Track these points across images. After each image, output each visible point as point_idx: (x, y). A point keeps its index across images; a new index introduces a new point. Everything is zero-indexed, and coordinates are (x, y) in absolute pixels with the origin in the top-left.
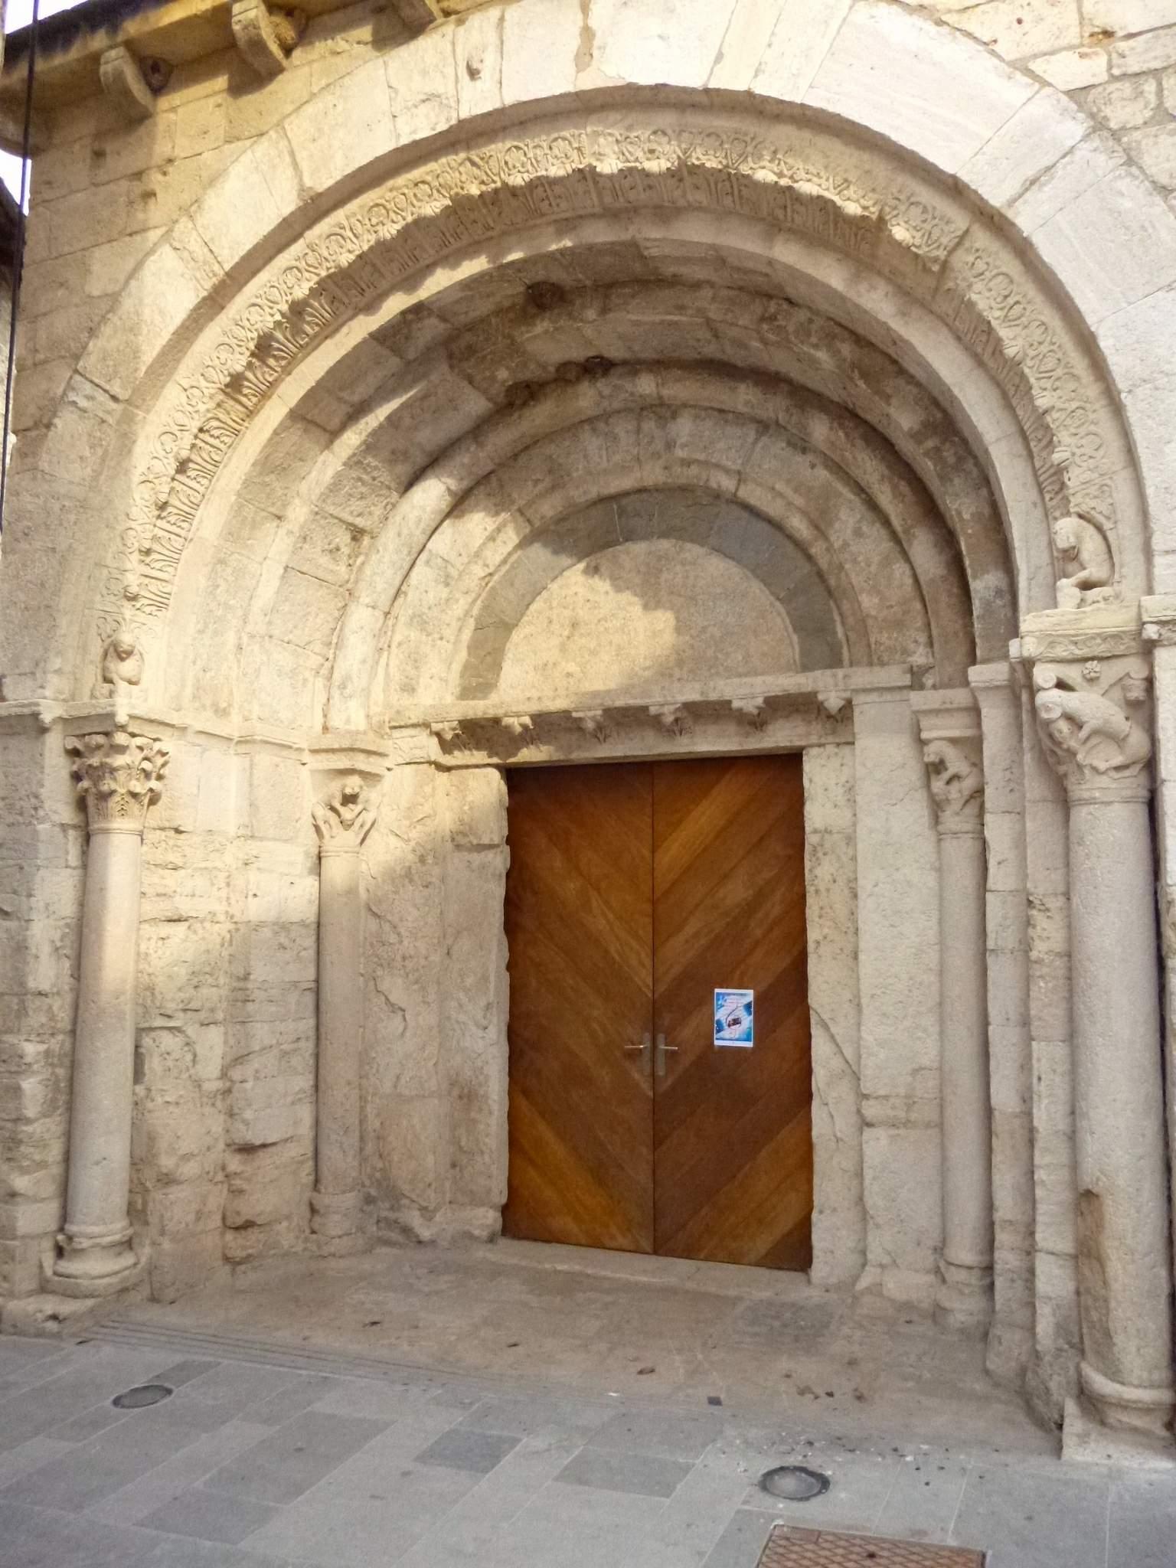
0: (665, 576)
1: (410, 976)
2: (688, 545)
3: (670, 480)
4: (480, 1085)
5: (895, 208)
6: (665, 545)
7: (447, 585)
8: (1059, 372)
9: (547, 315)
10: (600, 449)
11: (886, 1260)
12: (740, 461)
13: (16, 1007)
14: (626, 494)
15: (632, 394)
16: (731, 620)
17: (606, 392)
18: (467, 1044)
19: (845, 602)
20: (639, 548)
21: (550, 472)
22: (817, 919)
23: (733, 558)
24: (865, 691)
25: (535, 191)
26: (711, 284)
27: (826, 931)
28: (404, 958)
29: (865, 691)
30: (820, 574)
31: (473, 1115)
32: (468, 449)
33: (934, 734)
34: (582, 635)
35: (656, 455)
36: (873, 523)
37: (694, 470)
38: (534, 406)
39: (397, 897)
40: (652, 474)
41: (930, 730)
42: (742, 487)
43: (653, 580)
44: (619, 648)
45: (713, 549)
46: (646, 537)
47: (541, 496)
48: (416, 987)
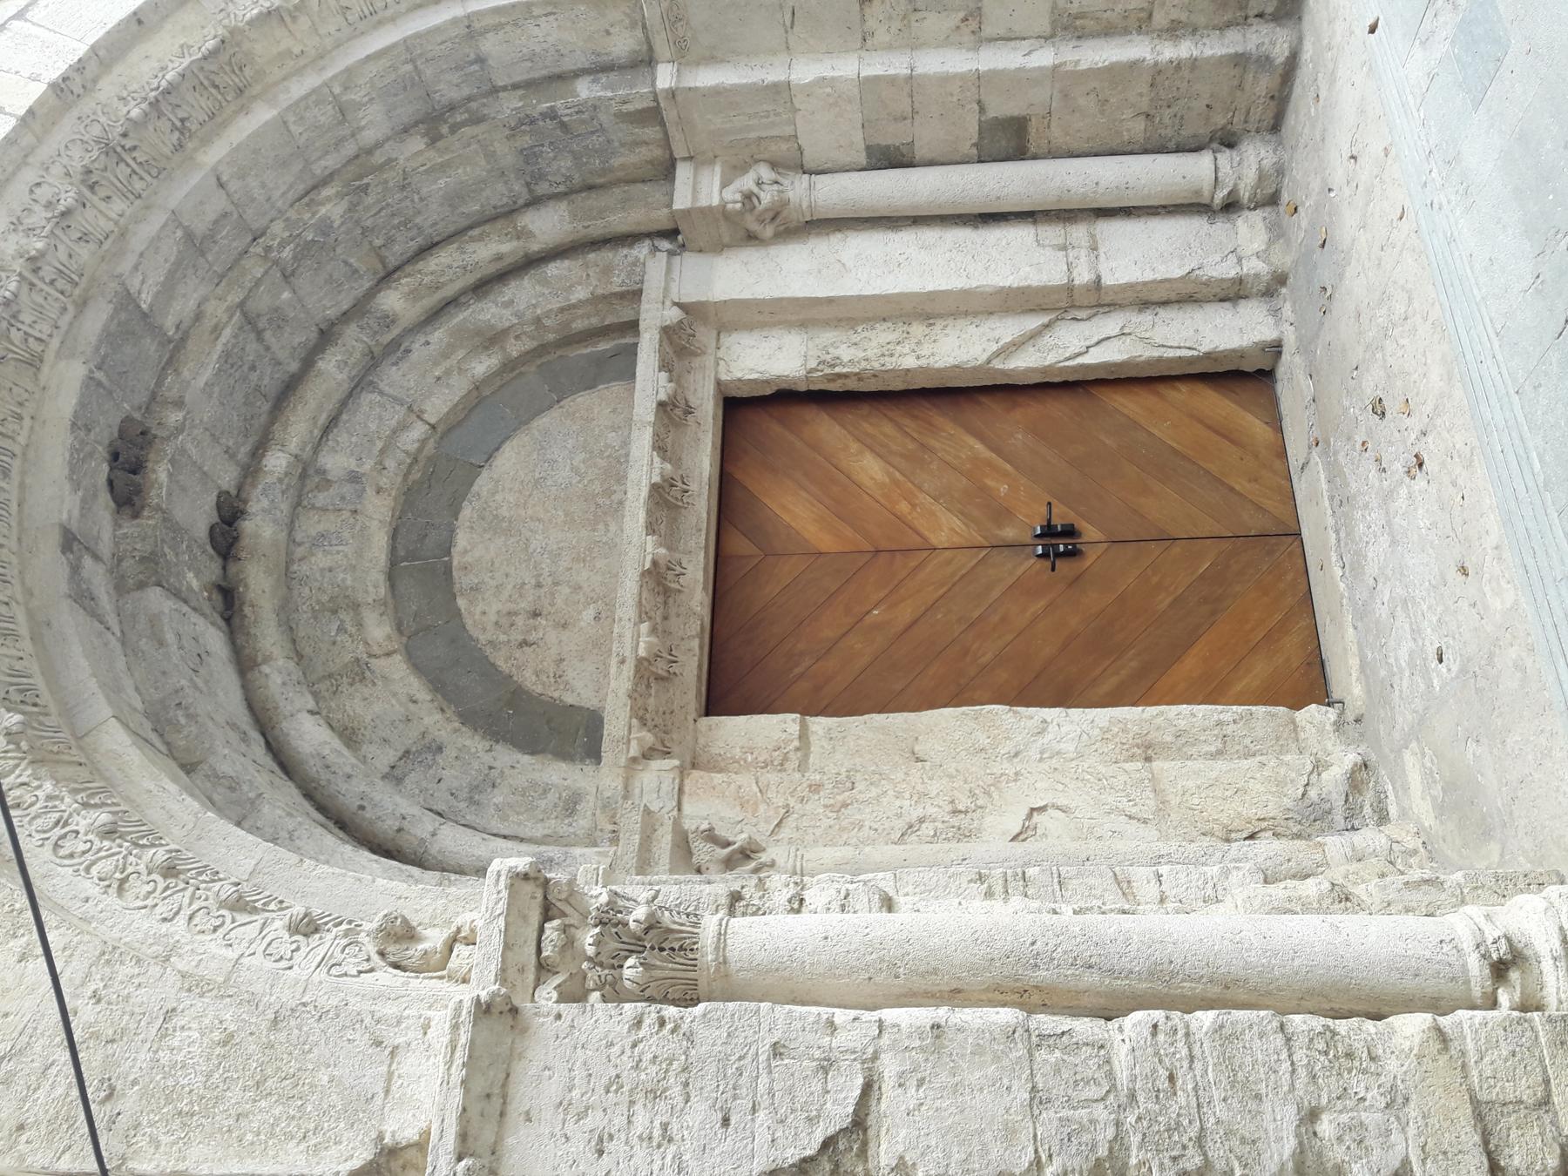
0: (504, 512)
1: (979, 803)
2: (475, 488)
5: (229, 15)
6: (467, 512)
9: (150, 465)
10: (329, 553)
11: (1232, 259)
12: (398, 408)
13: (1058, 1054)
14: (393, 550)
15: (280, 480)
16: (570, 443)
17: (265, 503)
18: (1072, 749)
19: (574, 326)
20: (462, 540)
21: (334, 612)
22: (894, 359)
23: (503, 442)
25: (12, 336)
26: (205, 299)
28: (955, 812)
30: (542, 349)
32: (266, 675)
34: (552, 605)
35: (360, 495)
36: (501, 292)
37: (390, 464)
38: (246, 586)
39: (867, 823)
40: (379, 510)
41: (711, 198)
42: (426, 416)
43: (505, 525)
44: (576, 560)
45: (487, 461)
46: (452, 531)
47: (360, 625)
48: (995, 795)
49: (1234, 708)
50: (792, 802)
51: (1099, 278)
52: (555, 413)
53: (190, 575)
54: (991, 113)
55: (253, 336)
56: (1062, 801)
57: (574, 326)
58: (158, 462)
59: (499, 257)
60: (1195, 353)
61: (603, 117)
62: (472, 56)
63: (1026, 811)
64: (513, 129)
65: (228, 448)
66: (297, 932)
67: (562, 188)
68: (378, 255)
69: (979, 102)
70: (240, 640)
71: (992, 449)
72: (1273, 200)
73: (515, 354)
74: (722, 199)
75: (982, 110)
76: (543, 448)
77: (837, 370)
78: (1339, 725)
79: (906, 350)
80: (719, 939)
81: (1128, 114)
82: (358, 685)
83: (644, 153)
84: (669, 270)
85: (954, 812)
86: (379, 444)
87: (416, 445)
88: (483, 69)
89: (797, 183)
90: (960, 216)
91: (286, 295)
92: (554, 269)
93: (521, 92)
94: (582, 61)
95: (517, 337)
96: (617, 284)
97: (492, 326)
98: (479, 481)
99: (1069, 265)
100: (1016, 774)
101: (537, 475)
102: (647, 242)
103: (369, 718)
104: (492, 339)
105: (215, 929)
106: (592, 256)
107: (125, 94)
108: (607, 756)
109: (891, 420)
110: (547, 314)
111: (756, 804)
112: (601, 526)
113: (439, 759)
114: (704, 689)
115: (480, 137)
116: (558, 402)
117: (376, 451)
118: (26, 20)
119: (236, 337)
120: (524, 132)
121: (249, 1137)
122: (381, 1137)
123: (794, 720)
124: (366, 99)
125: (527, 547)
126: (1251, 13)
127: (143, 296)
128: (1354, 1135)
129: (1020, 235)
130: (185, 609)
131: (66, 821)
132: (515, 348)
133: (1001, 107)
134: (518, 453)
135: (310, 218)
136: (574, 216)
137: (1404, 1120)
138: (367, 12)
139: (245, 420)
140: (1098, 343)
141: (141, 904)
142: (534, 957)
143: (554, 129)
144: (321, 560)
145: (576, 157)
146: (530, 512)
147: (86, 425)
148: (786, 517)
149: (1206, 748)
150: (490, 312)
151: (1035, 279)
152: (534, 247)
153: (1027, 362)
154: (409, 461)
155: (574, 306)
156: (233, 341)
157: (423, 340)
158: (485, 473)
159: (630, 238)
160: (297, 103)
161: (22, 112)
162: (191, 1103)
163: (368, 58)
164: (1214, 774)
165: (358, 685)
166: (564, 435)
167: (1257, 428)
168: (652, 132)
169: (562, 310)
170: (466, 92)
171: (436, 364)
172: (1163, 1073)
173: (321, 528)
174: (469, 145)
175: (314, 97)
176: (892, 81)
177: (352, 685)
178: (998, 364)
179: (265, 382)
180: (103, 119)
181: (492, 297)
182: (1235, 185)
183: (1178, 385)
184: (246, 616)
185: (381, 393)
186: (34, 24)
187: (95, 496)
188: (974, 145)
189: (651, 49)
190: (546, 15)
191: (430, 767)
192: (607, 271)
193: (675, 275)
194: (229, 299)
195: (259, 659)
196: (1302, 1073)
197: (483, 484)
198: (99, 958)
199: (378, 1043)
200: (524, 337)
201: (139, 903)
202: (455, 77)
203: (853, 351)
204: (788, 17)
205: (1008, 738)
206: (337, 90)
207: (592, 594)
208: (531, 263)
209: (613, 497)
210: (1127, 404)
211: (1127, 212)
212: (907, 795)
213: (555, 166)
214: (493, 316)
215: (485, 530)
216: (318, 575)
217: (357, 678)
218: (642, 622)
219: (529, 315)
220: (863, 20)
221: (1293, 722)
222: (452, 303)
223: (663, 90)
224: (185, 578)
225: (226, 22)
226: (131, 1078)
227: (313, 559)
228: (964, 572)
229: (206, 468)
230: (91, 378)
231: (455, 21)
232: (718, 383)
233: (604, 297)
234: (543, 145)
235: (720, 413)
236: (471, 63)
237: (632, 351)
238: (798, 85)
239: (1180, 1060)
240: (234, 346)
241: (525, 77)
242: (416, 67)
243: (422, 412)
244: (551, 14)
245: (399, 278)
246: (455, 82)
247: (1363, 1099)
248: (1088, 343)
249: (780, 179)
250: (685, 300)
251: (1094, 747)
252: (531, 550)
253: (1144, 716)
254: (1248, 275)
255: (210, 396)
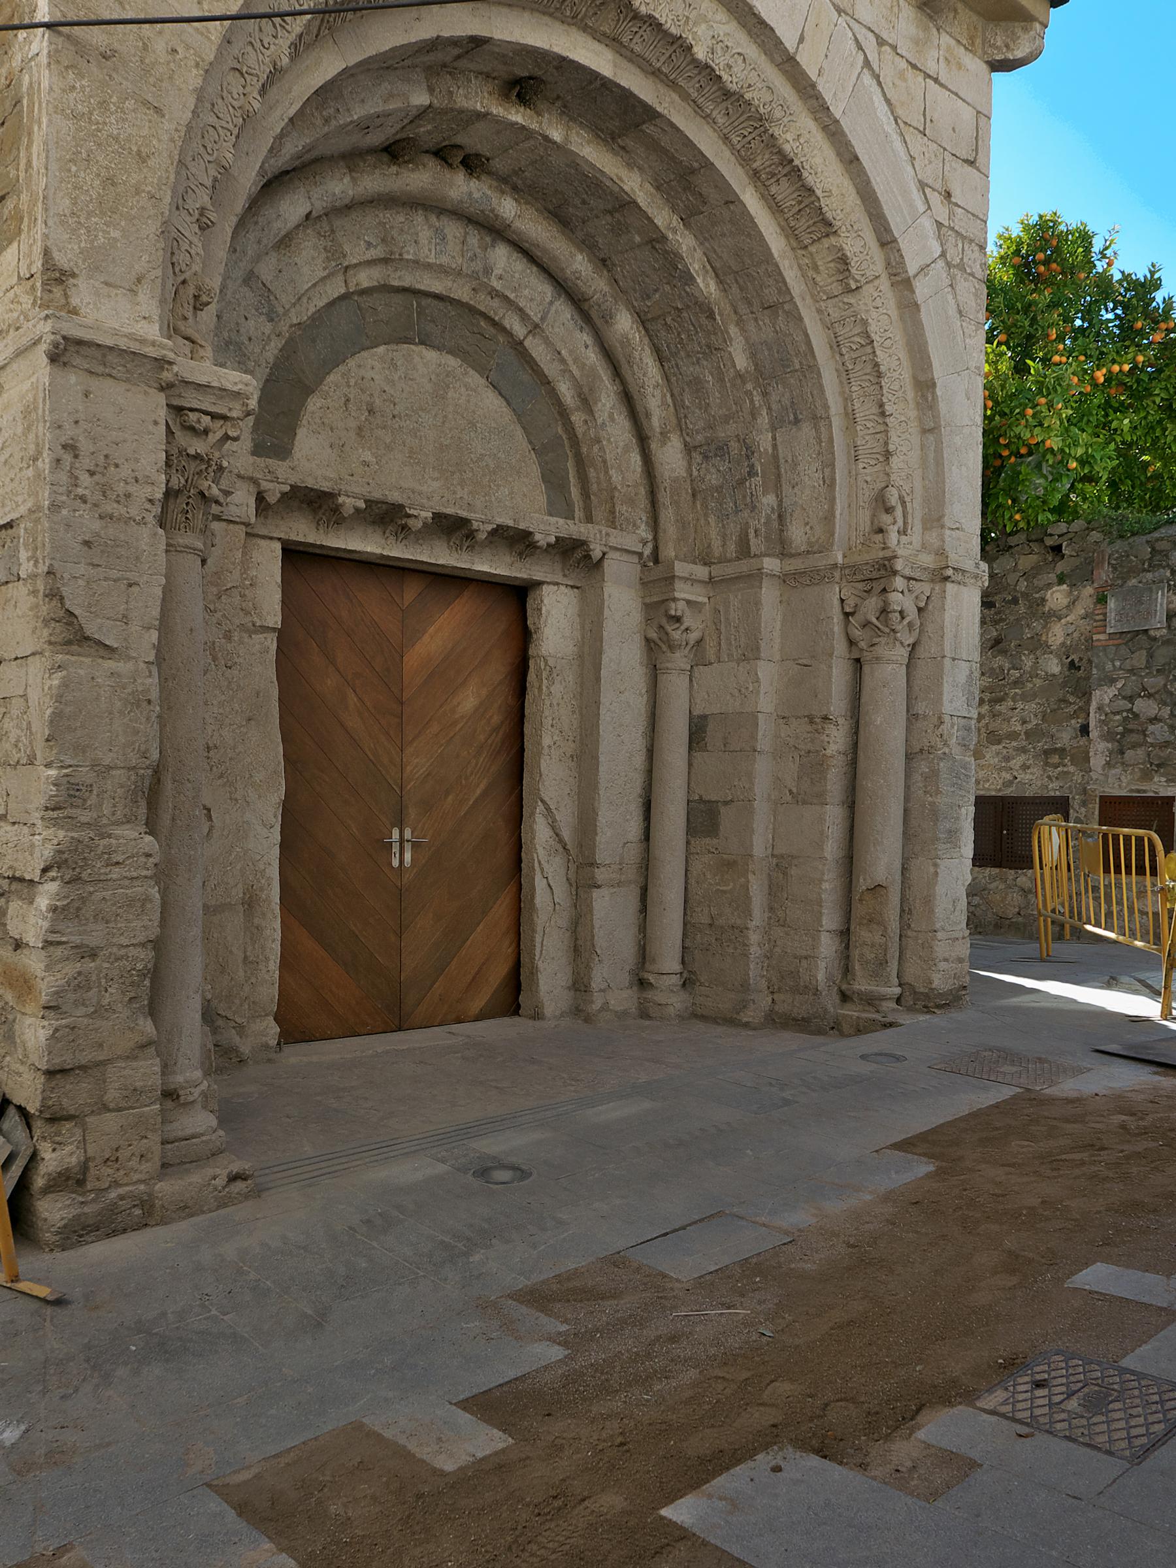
2: (472, 372)
3: (471, 302)
4: (262, 889)
6: (452, 362)
7: (271, 320)
8: (900, 394)
16: (501, 455)
19: (592, 470)
20: (431, 355)
23: (506, 400)
24: (616, 549)
27: (555, 738)
29: (616, 549)
31: (256, 921)
32: (342, 179)
33: (682, 595)
38: (413, 170)
42: (530, 338)
46: (438, 348)
48: (220, 782)
49: (277, 972)
50: (219, 615)
51: (599, 887)
52: (525, 445)
53: (429, 127)
54: (723, 809)
55: (609, 207)
56: (216, 834)
57: (592, 470)
58: (523, 116)
59: (648, 415)
60: (537, 958)
61: (746, 514)
62: (800, 417)
63: (209, 806)
64: (744, 440)
65: (523, 172)
66: (201, 215)
67: (695, 473)
68: (659, 316)
69: (732, 801)
70: (371, 159)
71: (476, 801)
72: (644, 1014)
73: (573, 418)
74: (679, 600)
75: (726, 803)
76: (499, 432)
77: (545, 681)
78: (266, 1046)
79: (555, 738)
80: (191, 548)
81: (714, 911)
82: (324, 255)
83: (716, 544)
84: (634, 553)
85: (208, 748)
86: (512, 296)
87: (508, 327)
88: (790, 422)
89: (685, 660)
90: (650, 785)
91: (637, 239)
92: (636, 459)
93: (770, 451)
94: (787, 502)
95: (586, 422)
96: (622, 509)
97: (596, 403)
98: (477, 375)
99: (609, 865)
100: (236, 800)
101: (478, 425)
102: (650, 537)
103: (298, 262)
104: (586, 402)
105: (205, 147)
106: (642, 491)
107: (802, 141)
108: (261, 461)
109: (502, 723)
110: (602, 449)
111: (217, 585)
112: (436, 475)
113: (263, 318)
114: (301, 548)
115: (740, 413)
116: (533, 449)
117: (508, 293)
118: (862, 68)
119: (611, 193)
120: (741, 450)
121: (74, 169)
122: (74, 275)
123: (276, 622)
124: (778, 329)
125: (422, 410)
126: (775, 996)
127: (652, 128)
128: (83, 983)
129: (634, 828)
130: (406, 121)
131: (284, 27)
132: (577, 418)
133: (727, 817)
134: (496, 412)
135: (694, 269)
136: (675, 480)
137: (94, 1016)
138: (839, 339)
139: (543, 188)
140: (549, 885)
141: (224, 87)
142: (188, 406)
143: (741, 474)
144: (425, 234)
145: (719, 489)
146: (450, 416)
147: (561, 67)
148: (431, 630)
149: (250, 948)
150: (607, 401)
151: (601, 839)
152: (653, 446)
153: (539, 833)
154: (496, 318)
155: (607, 472)
156: (608, 191)
157: (589, 343)
158: (483, 381)
159: (655, 523)
160: (780, 274)
161: (798, 58)
162: (98, 123)
163: (807, 335)
164: (234, 950)
165: (324, 255)
166: (508, 452)
167: (478, 1003)
168: (732, 548)
169: (605, 462)
170: (774, 407)
171: (571, 352)
172: (120, 858)
173: (449, 237)
174: (735, 404)
175: (784, 288)
176: (753, 737)
177: (325, 249)
178: (540, 807)
179: (571, 209)
180: (785, 120)
181: (617, 406)
182: (657, 988)
183: (514, 945)
184: (389, 167)
185: (551, 303)
186: (859, 74)
187: (505, 63)
188: (701, 797)
189: (792, 556)
190: (823, 478)
191: (257, 310)
192: (631, 502)
193: (625, 557)
194: (641, 194)
195: (354, 174)
196: (123, 952)
197: (475, 379)
198: (200, 57)
199: (139, 280)
200: (586, 427)
201: (225, 84)
202: (786, 401)
203: (559, 695)
204: (805, 662)
205: (260, 797)
206: (786, 307)
207: (384, 461)
208: (642, 439)
209: (459, 487)
210: (501, 908)
211: (644, 909)
212: (221, 711)
213: (713, 470)
214: (604, 405)
215: (438, 375)
216: (413, 230)
217: (330, 254)
218: (366, 501)
219: (603, 434)
220: (797, 717)
221: (267, 1015)
222: (617, 373)
223: (762, 561)
224: (429, 123)
225: (844, 229)
226: (114, 75)
227: (425, 227)
228: (384, 772)
229: (511, 151)
230: (597, 77)
231: (826, 407)
232: (539, 584)
233: (612, 498)
234: (730, 462)
235: (516, 583)
236: (795, 414)
237: (570, 516)
238: (757, 665)
239: (130, 871)
240: (604, 191)
241: (781, 456)
242: (796, 371)
243: (534, 336)
244: (824, 482)
245: (640, 332)
246: (783, 399)
247: (106, 991)
248: (549, 878)
249: (689, 647)
250: (606, 563)
251: (250, 864)
252: (420, 413)
253: (273, 904)
254: (592, 996)
255: (567, 165)
